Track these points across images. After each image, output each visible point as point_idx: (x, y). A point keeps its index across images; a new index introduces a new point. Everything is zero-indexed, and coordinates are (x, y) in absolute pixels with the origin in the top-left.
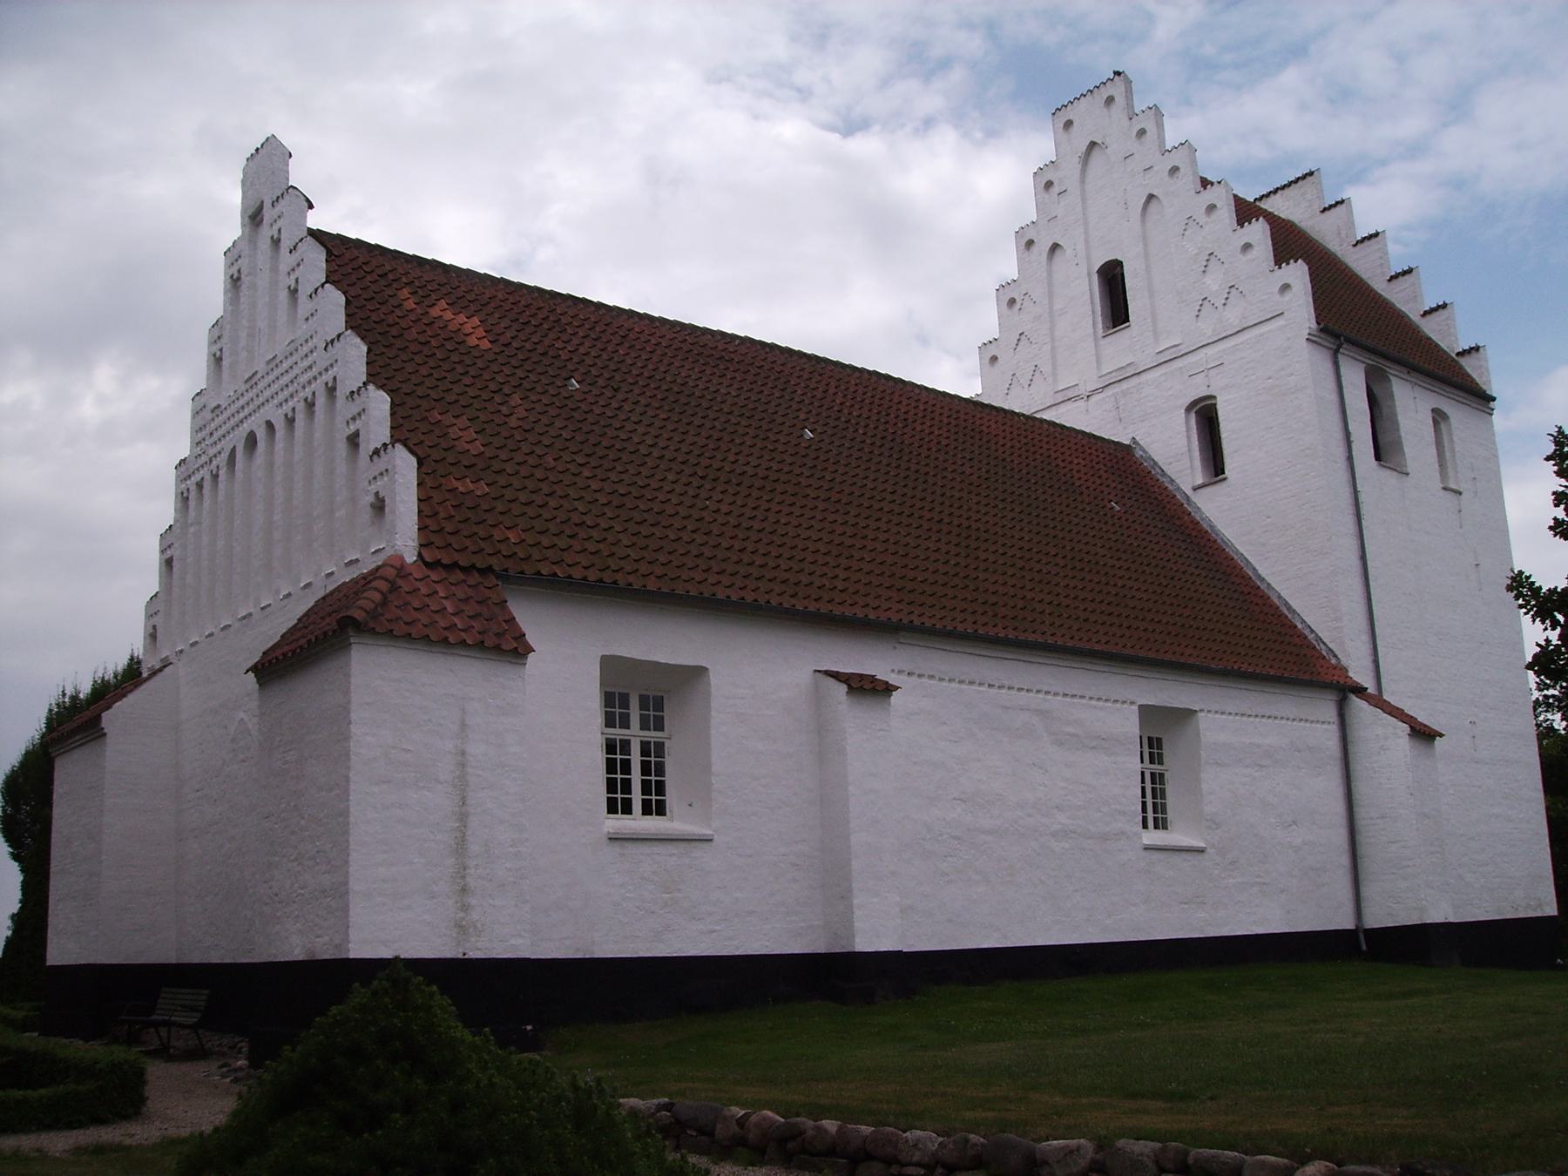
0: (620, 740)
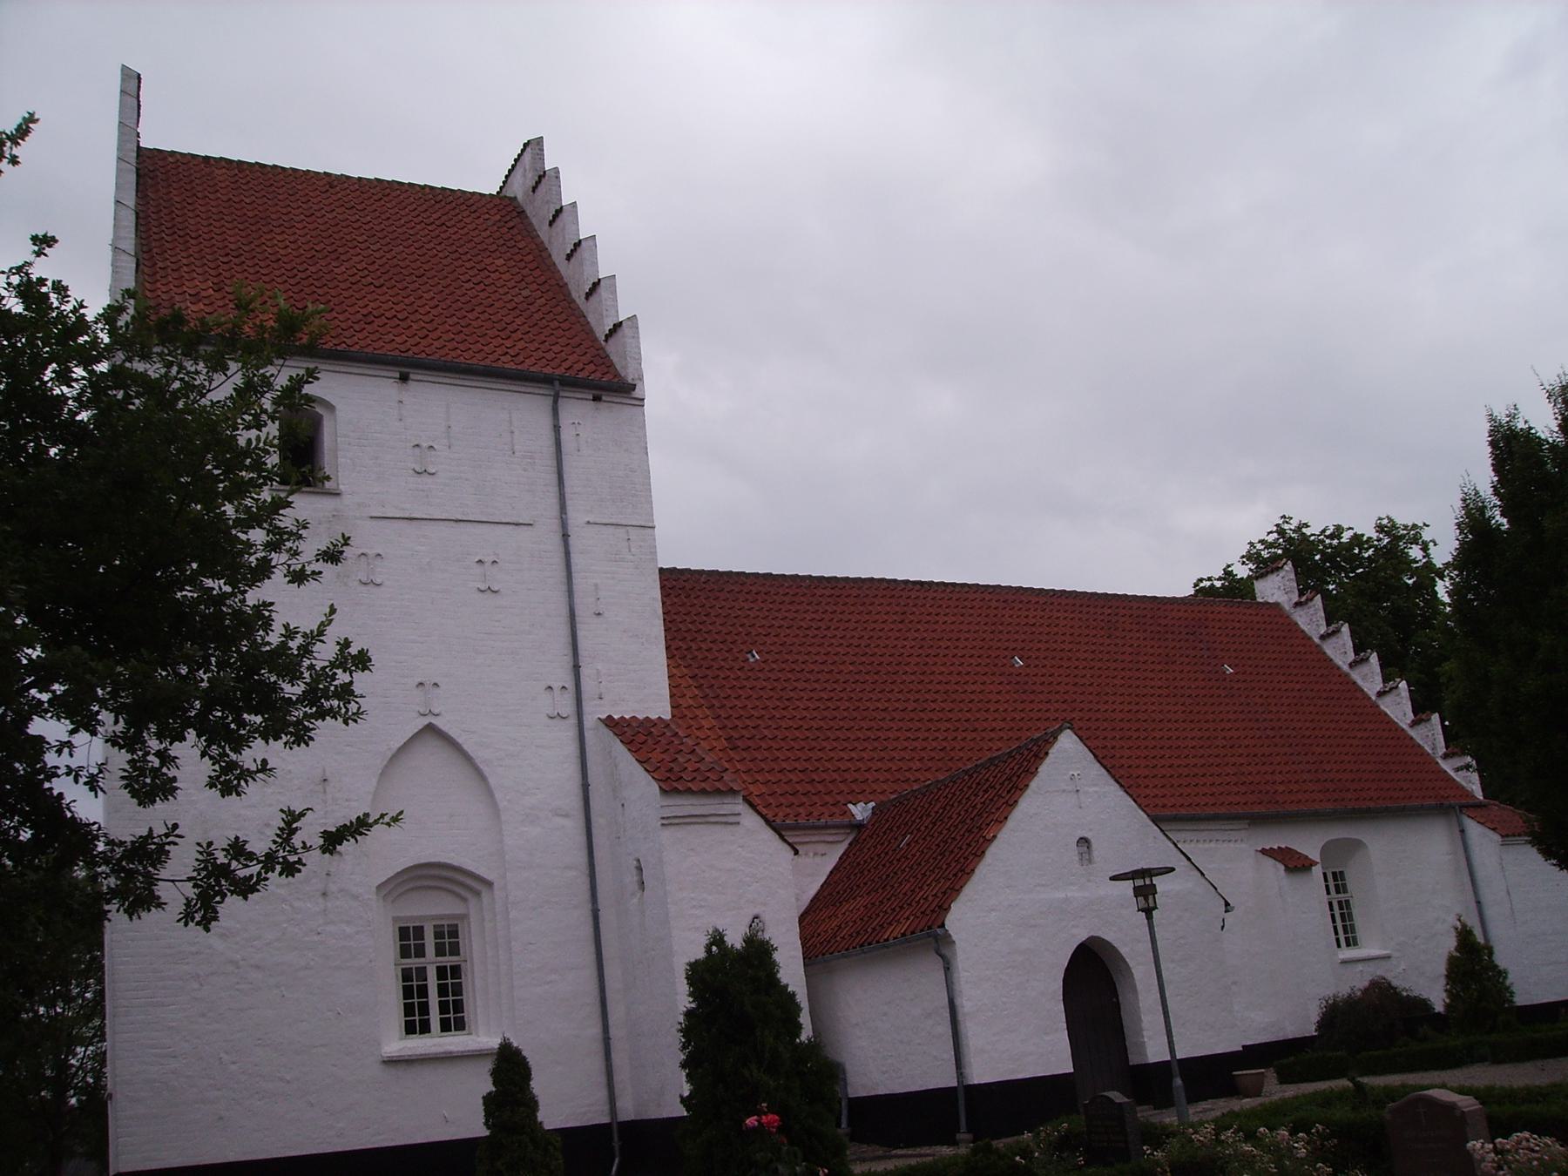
0: (451, 966)
